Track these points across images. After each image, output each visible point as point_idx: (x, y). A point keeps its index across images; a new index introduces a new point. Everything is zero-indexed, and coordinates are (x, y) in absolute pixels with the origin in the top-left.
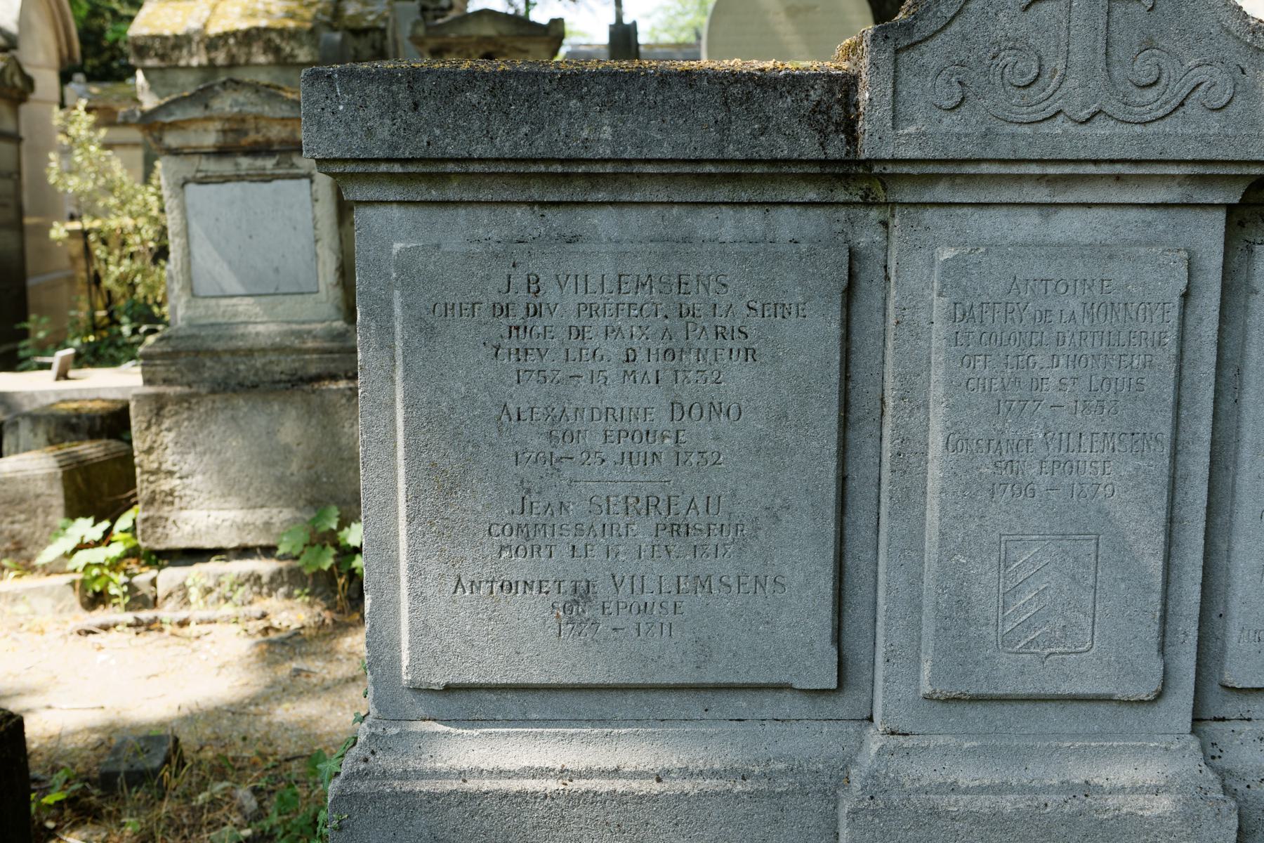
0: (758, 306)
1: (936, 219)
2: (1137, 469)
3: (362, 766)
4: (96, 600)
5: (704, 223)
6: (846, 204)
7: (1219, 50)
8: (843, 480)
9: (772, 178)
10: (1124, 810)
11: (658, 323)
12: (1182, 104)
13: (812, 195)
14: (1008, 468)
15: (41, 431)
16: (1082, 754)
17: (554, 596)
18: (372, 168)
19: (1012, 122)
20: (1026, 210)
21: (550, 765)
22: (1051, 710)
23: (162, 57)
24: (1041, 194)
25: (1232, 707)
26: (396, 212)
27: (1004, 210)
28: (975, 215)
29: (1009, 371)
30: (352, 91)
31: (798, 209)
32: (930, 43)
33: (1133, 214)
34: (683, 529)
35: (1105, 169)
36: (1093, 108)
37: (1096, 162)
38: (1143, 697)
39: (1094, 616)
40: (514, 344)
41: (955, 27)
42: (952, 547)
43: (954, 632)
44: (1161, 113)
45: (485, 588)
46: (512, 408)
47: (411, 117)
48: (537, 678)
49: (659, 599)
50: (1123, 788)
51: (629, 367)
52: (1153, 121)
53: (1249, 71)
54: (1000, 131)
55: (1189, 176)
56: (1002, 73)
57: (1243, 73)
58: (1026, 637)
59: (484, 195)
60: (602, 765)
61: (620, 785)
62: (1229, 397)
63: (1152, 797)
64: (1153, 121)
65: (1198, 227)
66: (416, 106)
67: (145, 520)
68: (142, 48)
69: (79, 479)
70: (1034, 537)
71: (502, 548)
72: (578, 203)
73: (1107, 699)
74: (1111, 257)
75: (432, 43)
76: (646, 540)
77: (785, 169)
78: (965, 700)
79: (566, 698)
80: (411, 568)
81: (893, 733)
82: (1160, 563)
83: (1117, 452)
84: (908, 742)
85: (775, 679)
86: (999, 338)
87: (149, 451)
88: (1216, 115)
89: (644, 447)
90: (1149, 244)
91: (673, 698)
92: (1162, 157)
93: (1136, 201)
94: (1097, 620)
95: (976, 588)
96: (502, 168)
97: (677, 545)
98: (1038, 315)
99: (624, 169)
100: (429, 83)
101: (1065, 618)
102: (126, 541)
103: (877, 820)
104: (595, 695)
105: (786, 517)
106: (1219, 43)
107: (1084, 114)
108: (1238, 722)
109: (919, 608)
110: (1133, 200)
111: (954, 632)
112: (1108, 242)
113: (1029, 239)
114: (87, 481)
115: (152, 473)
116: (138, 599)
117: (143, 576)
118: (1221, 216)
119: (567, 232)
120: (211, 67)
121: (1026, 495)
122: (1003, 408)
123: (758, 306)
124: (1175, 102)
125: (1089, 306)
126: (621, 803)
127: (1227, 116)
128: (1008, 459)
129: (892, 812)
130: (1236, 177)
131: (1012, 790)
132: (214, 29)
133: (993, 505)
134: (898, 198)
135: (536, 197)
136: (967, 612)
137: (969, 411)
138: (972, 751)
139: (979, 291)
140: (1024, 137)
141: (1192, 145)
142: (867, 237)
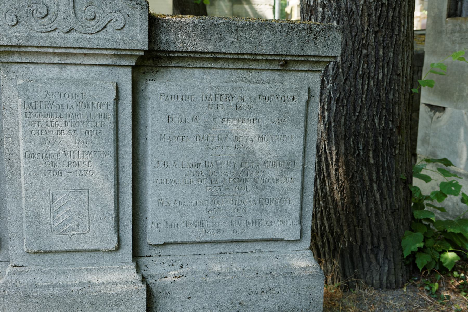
1: (16, 68)
2: (102, 164)
7: (118, 7)
10: (103, 292)
12: (105, 27)
14: (51, 164)
16: (89, 271)
19: (38, 32)
20: (53, 66)
22: (77, 255)
24: (57, 60)
25: (153, 252)
27: (44, 66)
28: (32, 68)
29: (48, 127)
33: (95, 68)
35: (78, 51)
36: (70, 27)
37: (74, 48)
38: (110, 249)
39: (89, 220)
42: (31, 195)
43: (34, 227)
44: (97, 30)
50: (103, 283)
52: (94, 33)
53: (131, 16)
54: (33, 35)
55: (112, 55)
56: (33, 13)
57: (129, 16)
58: (63, 228)
59: (201, 65)
62: (144, 138)
63: (114, 286)
64: (94, 33)
65: (121, 74)
70: (63, 191)
73: (97, 251)
74: (85, 84)
78: (41, 253)
81: (15, 266)
82: (113, 200)
83: (93, 158)
86: (43, 115)
88: (119, 32)
90: (103, 80)
92: (98, 47)
93: (95, 64)
94: (90, 221)
95: (41, 210)
98: (58, 106)
101: (78, 221)
103: (5, 300)
106: (118, 4)
107: (67, 30)
108: (155, 257)
109: (21, 218)
110: (94, 63)
112: (86, 79)
113: (55, 77)
118: (130, 70)
121: (58, 174)
122: (47, 142)
124: (102, 26)
125: (78, 103)
127: (123, 32)
128: (50, 161)
129: (11, 297)
130: (131, 56)
131: (60, 286)
133: (46, 179)
136: (39, 220)
137: (33, 143)
138: (46, 272)
139: (33, 97)
140: (43, 37)
141: (109, 43)
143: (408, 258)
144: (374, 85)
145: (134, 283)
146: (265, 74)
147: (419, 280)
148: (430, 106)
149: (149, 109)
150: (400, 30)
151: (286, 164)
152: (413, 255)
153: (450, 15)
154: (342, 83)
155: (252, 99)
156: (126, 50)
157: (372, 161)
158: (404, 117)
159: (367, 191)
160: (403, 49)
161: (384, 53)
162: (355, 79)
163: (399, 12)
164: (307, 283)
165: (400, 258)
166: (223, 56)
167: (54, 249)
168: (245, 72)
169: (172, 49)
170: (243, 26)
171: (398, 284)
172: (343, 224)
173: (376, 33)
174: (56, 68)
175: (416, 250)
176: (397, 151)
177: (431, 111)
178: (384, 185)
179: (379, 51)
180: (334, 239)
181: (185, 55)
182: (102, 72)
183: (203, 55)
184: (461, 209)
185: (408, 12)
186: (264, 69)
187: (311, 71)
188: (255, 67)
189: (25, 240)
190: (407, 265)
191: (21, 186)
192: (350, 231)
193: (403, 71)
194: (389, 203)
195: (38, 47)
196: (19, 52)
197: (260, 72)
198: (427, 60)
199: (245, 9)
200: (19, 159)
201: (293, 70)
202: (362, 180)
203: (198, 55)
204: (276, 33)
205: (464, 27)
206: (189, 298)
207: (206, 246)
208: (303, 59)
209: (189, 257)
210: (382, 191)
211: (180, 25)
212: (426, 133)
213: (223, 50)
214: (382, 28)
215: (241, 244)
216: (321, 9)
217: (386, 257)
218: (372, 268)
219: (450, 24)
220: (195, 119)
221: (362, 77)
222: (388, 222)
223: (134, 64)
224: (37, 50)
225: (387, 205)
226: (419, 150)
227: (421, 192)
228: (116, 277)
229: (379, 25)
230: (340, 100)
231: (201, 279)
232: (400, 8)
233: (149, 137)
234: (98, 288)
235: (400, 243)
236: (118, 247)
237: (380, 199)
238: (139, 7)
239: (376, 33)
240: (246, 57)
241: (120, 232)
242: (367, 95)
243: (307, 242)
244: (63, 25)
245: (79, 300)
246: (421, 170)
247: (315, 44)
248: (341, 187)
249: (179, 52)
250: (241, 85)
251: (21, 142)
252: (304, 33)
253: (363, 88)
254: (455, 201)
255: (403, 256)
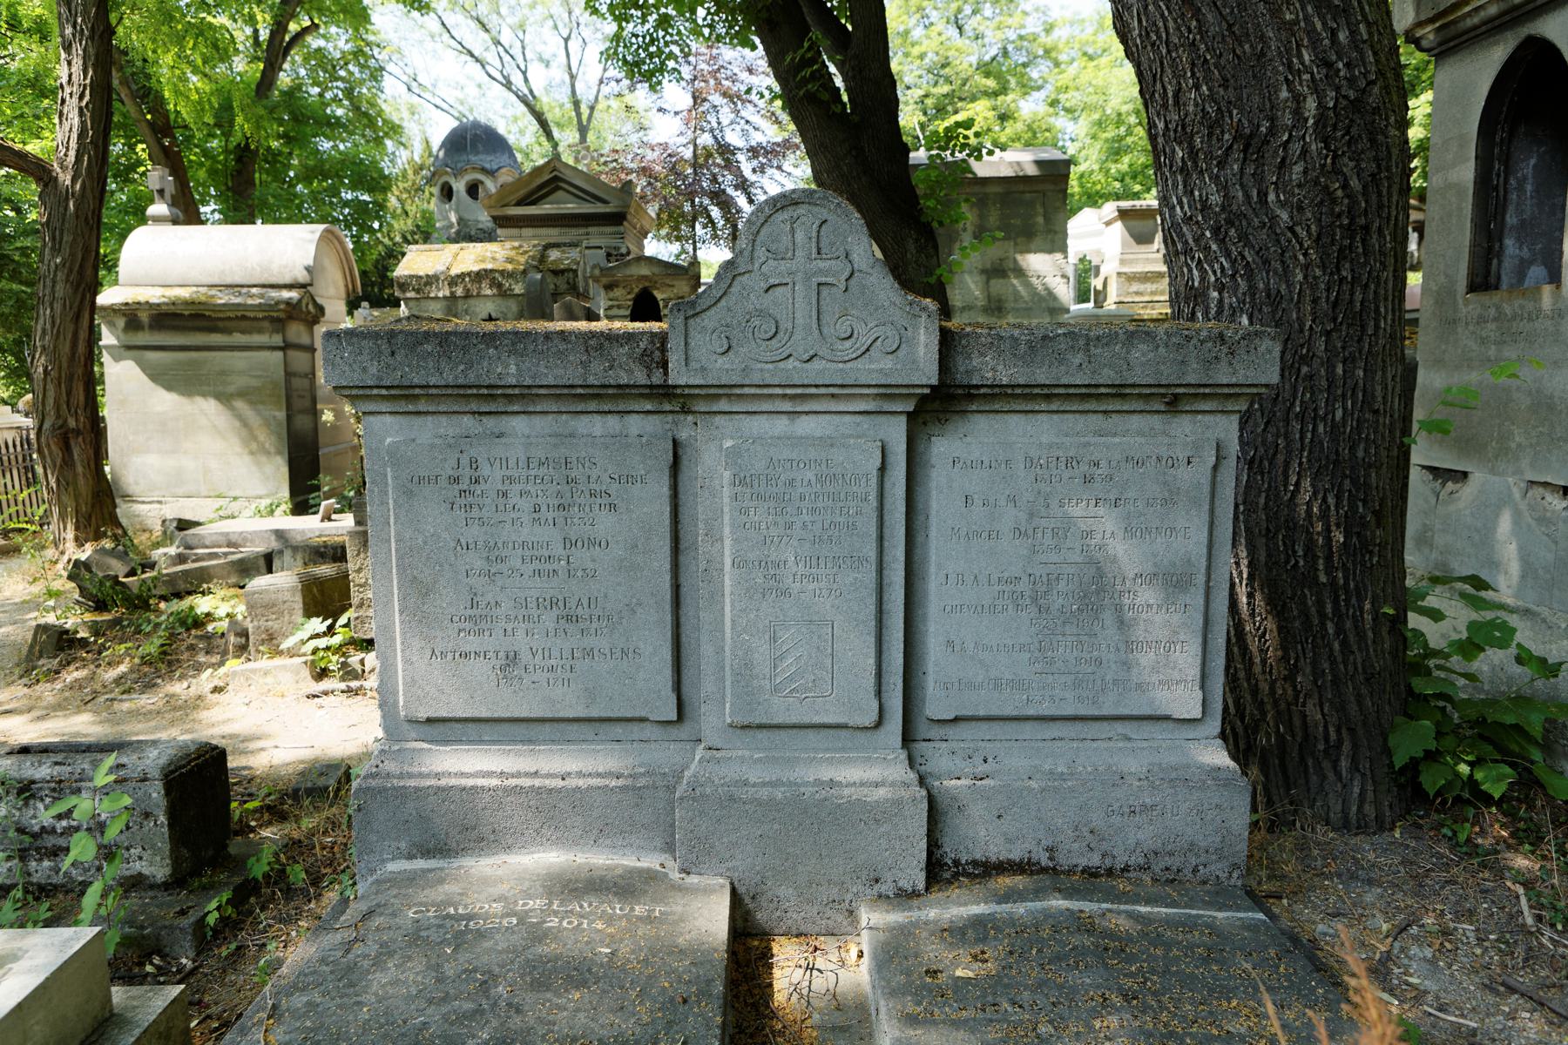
0: (616, 477)
3: (374, 770)
4: (322, 674)
5: (583, 425)
6: (672, 412)
8: (676, 588)
9: (622, 396)
11: (554, 488)
13: (649, 407)
15: (299, 557)
16: (830, 761)
17: (494, 661)
18: (368, 392)
20: (779, 416)
21: (494, 769)
22: (811, 734)
23: (418, 291)
24: (787, 406)
25: (935, 732)
26: (388, 419)
27: (765, 416)
28: (747, 421)
30: (353, 344)
31: (642, 416)
32: (708, 313)
33: (847, 418)
34: (574, 619)
35: (823, 391)
36: (811, 353)
37: (817, 386)
38: (867, 725)
40: (463, 501)
41: (723, 303)
43: (743, 683)
44: (854, 356)
45: (450, 656)
46: (463, 542)
47: (390, 360)
48: (485, 714)
49: (561, 663)
51: (536, 516)
59: (442, 408)
60: (527, 769)
61: (537, 782)
66: (393, 353)
67: (357, 618)
68: (403, 286)
69: (315, 590)
71: (460, 631)
72: (502, 413)
73: (844, 727)
74: (832, 445)
75: (605, 280)
76: (551, 626)
77: (627, 391)
79: (506, 726)
80: (403, 643)
84: (718, 755)
85: (637, 714)
87: (359, 570)
88: (890, 357)
89: (548, 566)
90: (859, 437)
91: (575, 726)
96: (449, 391)
97: (571, 628)
99: (526, 391)
100: (401, 338)
102: (345, 632)
104: (524, 725)
105: (640, 610)
107: (806, 357)
109: (723, 668)
111: (743, 683)
114: (322, 592)
115: (361, 586)
116: (349, 673)
117: (355, 659)
118: (904, 419)
119: (496, 431)
120: (453, 296)
123: (616, 477)
126: (538, 794)
131: (783, 784)
132: (454, 271)
134: (696, 409)
135: (475, 409)
138: (760, 760)
140: (768, 370)
142: (683, 435)
143: (1404, 769)
144: (1326, 432)
145: (906, 785)
146: (1136, 421)
147: (1427, 815)
148: (1434, 471)
149: (933, 484)
150: (1377, 327)
151: (1174, 579)
152: (1413, 766)
153: (1473, 288)
154: (1259, 430)
155: (1114, 464)
156: (902, 386)
157: (1323, 578)
158: (1388, 493)
159: (1314, 637)
160: (1384, 361)
161: (1344, 371)
162: (1287, 421)
163: (1375, 292)
164: (1216, 800)
165: (1386, 770)
166: (1062, 391)
167: (775, 721)
168: (1100, 416)
169: (975, 382)
170: (1098, 338)
171: (1383, 822)
172: (1266, 700)
173: (1328, 333)
174: (784, 420)
175: (1421, 754)
176: (1375, 559)
177: (1435, 479)
178: (1349, 624)
179: (1334, 367)
180: (1246, 729)
181: (997, 390)
182: (858, 424)
183: (1027, 391)
184: (1511, 678)
185: (1394, 291)
186: (1134, 412)
187: (1222, 411)
188: (1118, 408)
189: (728, 705)
190: (1401, 787)
191: (723, 615)
192: (1278, 713)
193: (1385, 404)
194: (1359, 660)
195: (760, 386)
196: (729, 396)
197: (1126, 416)
198: (1422, 376)
199: (1014, 285)
200: (722, 570)
201: (1187, 412)
202: (1305, 614)
203: (1019, 391)
204: (1158, 346)
205: (1508, 310)
206: (999, 817)
207: (1028, 726)
208: (1207, 391)
209: (998, 744)
210: (1346, 636)
211: (990, 340)
212: (1425, 525)
213: (1064, 381)
214: (1341, 323)
215: (1090, 723)
216: (1215, 294)
217: (1355, 767)
218: (1327, 787)
219: (1470, 306)
220: (1013, 500)
221: (1301, 417)
222: (1359, 697)
223: (911, 409)
224: (758, 391)
225: (1355, 663)
226: (1410, 558)
227: (1426, 641)
228: (874, 773)
229: (1334, 319)
230: (1257, 462)
231: (1019, 783)
232: (1378, 285)
233: (933, 533)
234: (846, 792)
235: (1385, 740)
236: (879, 724)
237: (1342, 652)
238: (924, 315)
239: (1328, 333)
240: (1103, 390)
241: (883, 695)
242: (1310, 452)
243: (1214, 725)
244: (801, 350)
245: (815, 810)
246: (1423, 598)
247: (1231, 364)
248: (1259, 628)
249: (986, 386)
250: (1093, 440)
251: (728, 542)
252: (1210, 344)
253: (1302, 438)
254: (1496, 662)
255: (1393, 767)
